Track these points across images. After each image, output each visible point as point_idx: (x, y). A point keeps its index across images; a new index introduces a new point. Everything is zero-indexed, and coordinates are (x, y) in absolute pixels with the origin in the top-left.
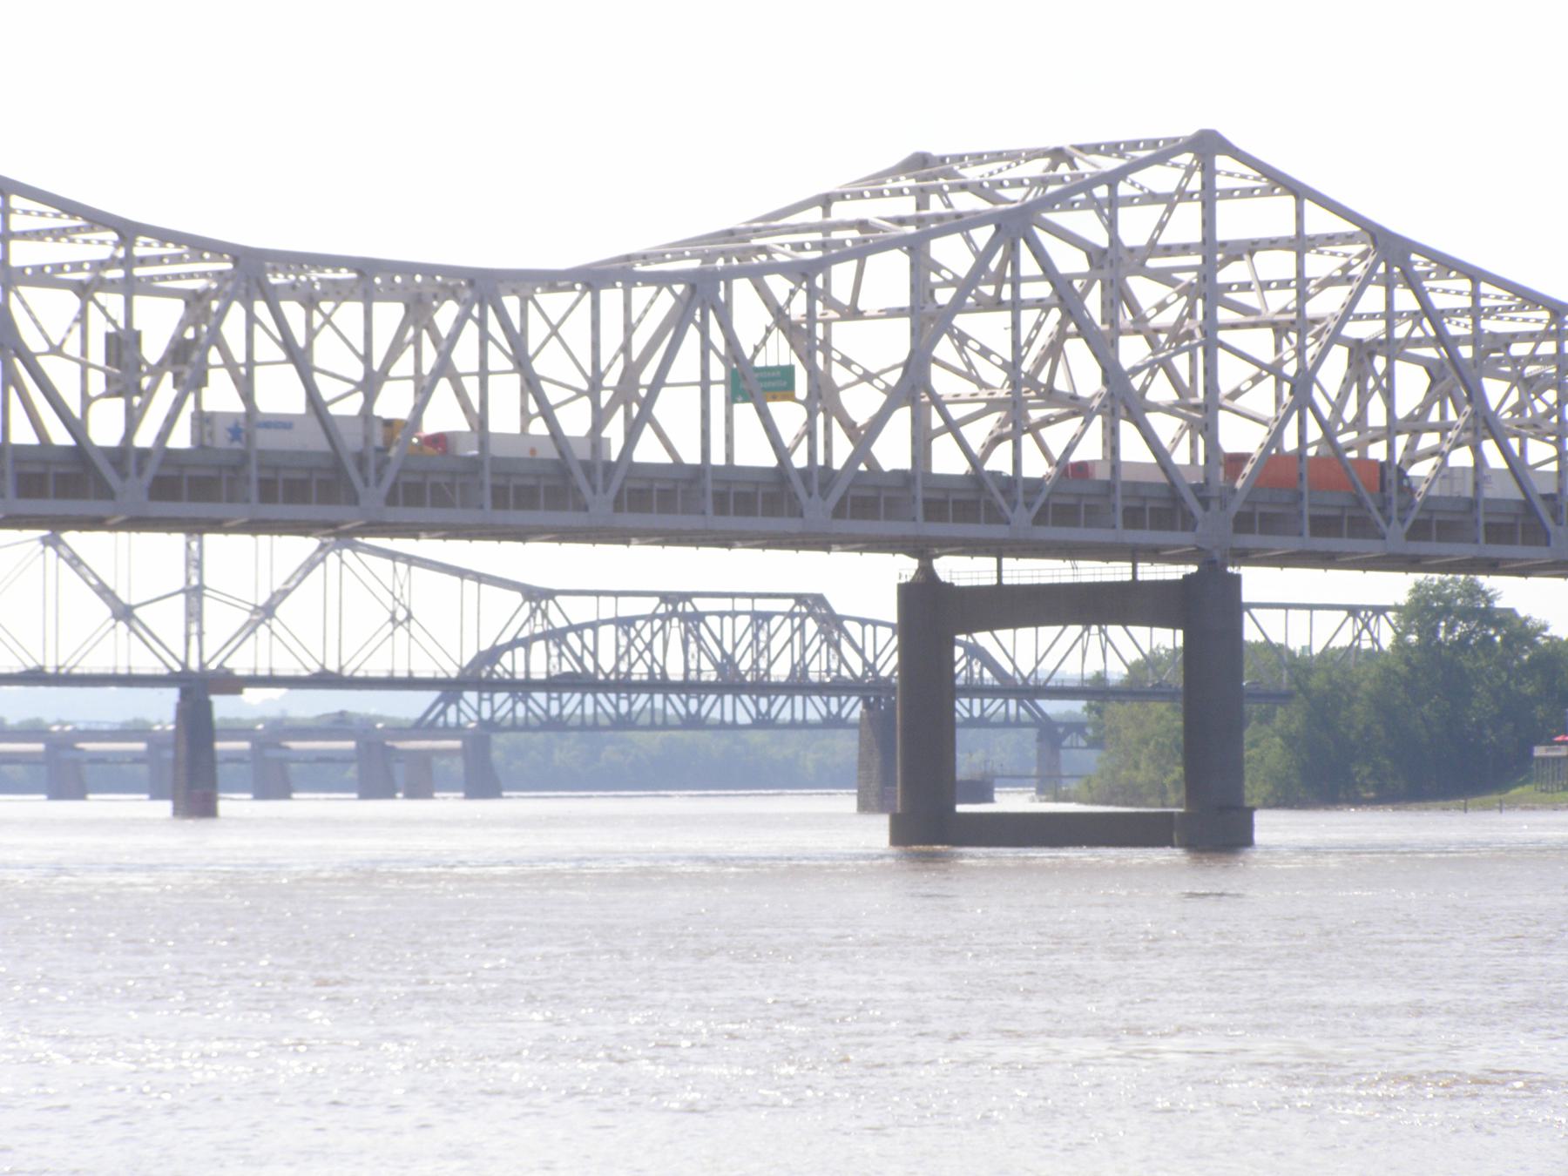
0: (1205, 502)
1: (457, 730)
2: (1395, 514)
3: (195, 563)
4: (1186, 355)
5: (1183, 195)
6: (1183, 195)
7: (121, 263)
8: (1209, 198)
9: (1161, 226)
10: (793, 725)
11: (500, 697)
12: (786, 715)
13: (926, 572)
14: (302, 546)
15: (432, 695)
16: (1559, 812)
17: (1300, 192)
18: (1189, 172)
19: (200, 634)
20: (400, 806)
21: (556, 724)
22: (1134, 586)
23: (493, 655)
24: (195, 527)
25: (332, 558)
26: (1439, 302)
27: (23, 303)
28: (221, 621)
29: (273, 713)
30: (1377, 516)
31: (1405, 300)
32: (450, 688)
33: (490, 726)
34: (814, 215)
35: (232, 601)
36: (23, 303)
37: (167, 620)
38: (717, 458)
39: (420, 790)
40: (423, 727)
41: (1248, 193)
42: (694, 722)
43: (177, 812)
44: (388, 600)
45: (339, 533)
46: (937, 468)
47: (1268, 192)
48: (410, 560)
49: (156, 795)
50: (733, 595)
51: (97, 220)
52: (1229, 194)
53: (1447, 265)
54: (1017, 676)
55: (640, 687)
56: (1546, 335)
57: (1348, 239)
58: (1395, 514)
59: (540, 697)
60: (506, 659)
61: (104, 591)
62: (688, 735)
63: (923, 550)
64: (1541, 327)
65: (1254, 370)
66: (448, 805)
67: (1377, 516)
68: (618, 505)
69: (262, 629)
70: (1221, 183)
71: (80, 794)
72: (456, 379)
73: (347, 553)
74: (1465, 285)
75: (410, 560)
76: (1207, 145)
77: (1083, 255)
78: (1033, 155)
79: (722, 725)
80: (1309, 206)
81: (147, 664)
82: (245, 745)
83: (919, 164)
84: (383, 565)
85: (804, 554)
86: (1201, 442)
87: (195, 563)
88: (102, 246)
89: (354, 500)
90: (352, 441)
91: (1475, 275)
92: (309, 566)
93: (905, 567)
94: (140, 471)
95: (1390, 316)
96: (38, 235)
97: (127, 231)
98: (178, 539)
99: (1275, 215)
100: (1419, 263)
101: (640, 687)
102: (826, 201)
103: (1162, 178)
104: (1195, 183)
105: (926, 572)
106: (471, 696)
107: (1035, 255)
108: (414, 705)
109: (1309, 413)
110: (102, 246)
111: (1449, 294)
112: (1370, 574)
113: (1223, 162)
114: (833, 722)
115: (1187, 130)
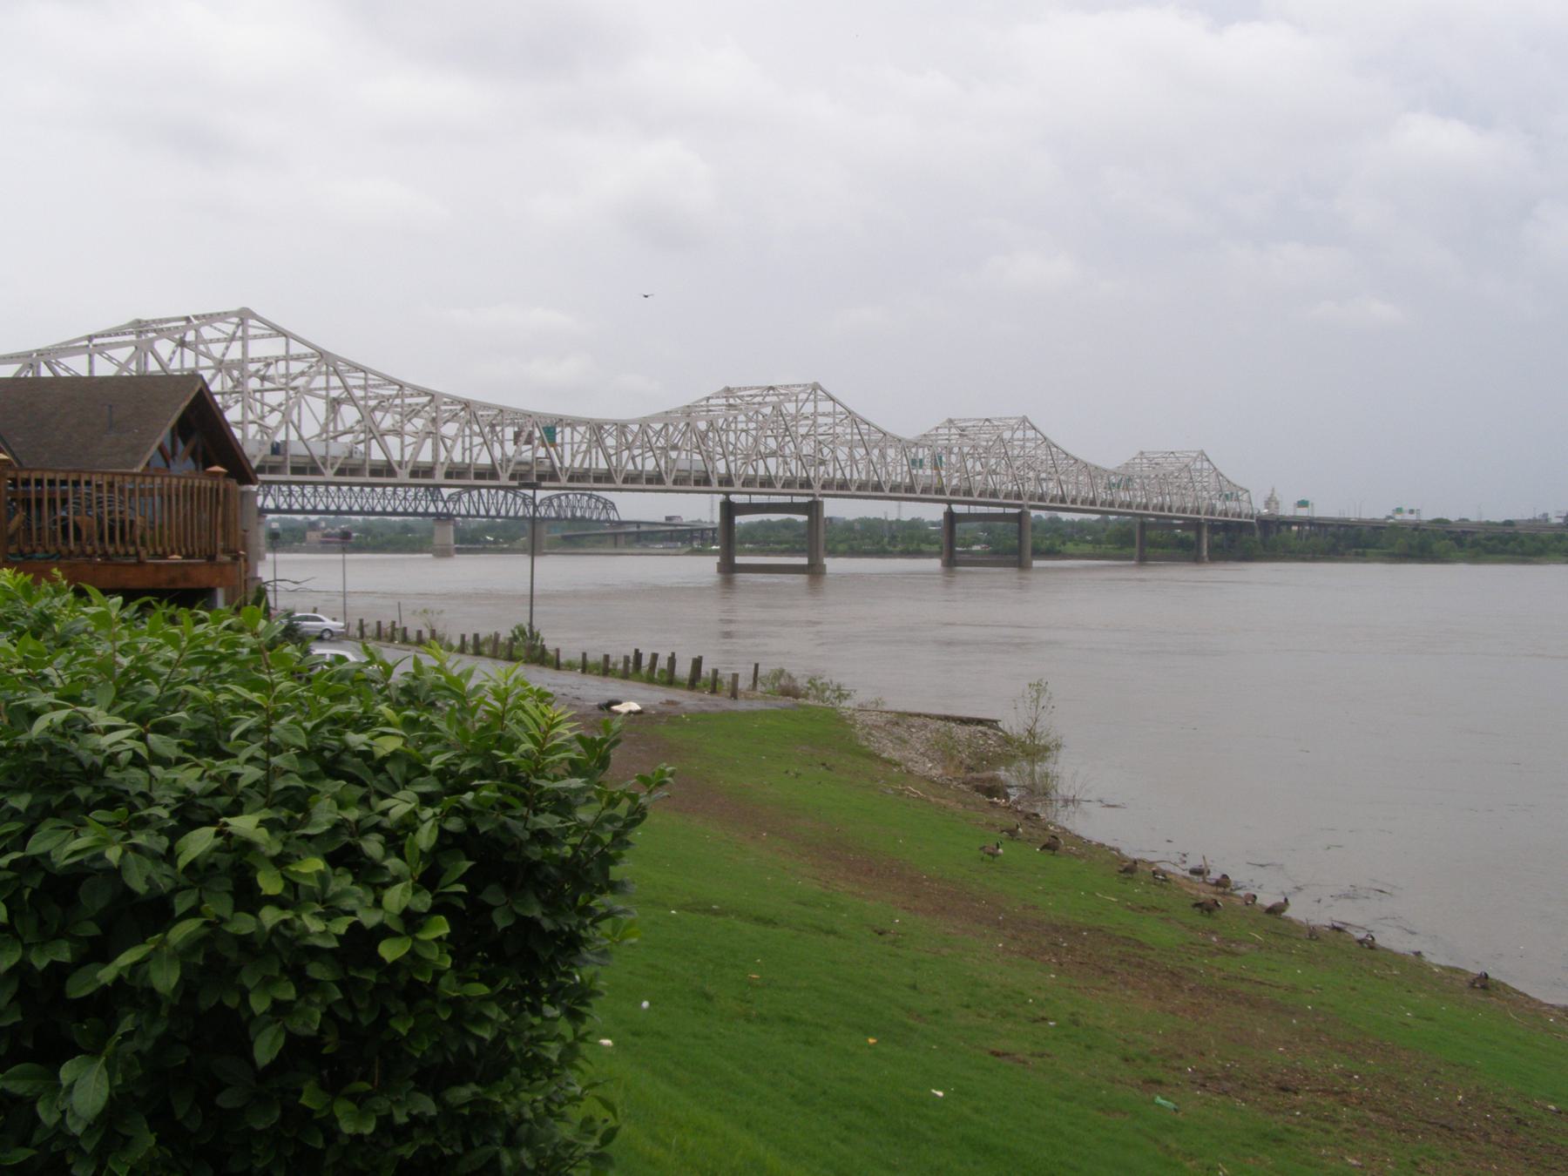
2: (329, 466)
5: (232, 338)
8: (244, 339)
13: (950, 508)
16: (1201, 567)
18: (810, 394)
22: (1004, 514)
27: (308, 406)
31: (335, 381)
36: (308, 406)
38: (594, 466)
41: (263, 336)
47: (277, 336)
53: (357, 368)
56: (397, 396)
57: (313, 356)
58: (329, 466)
64: (395, 392)
67: (322, 467)
70: (252, 332)
74: (362, 375)
76: (244, 316)
78: (758, 388)
95: (852, 434)
99: (275, 347)
100: (342, 367)
107: (157, 359)
111: (354, 380)
113: (252, 322)
115: (235, 308)
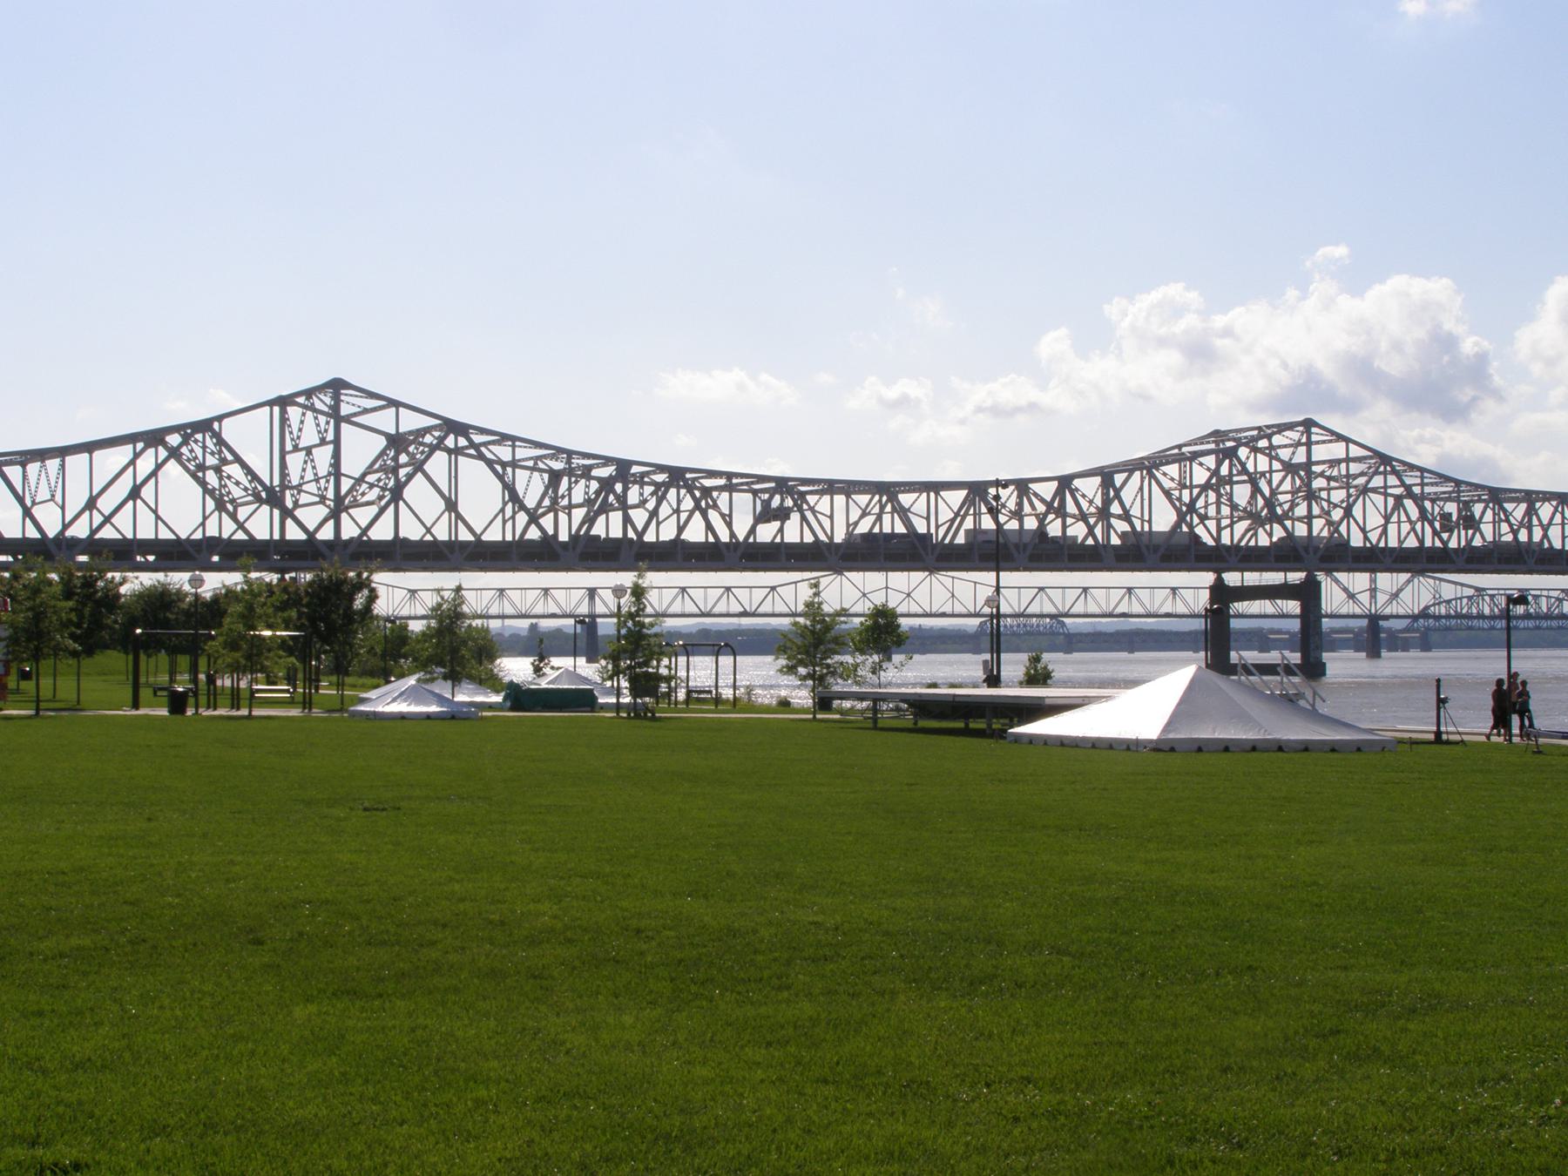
0: (1018, 550)
1: (1417, 630)
3: (1373, 581)
4: (1482, 505)
5: (1299, 444)
6: (1299, 444)
7: (1457, 492)
8: (1309, 444)
9: (1294, 453)
10: (1524, 629)
11: (1431, 621)
12: (1522, 626)
13: (1219, 581)
14: (1404, 577)
15: (1410, 620)
17: (1347, 440)
19: (1376, 603)
20: (1399, 654)
21: (1448, 629)
23: (1427, 608)
24: (1373, 571)
25: (1416, 580)
26: (1408, 481)
28: (1382, 598)
29: (1270, 626)
30: (922, 552)
32: (1415, 618)
33: (1428, 629)
34: (1176, 451)
35: (1384, 592)
37: (1364, 598)
39: (1405, 649)
40: (1406, 630)
42: (1470, 628)
43: (1367, 656)
44: (1432, 591)
45: (1421, 572)
46: (1112, 543)
47: (1337, 441)
48: (1441, 580)
49: (1357, 650)
50: (1498, 589)
51: (1448, 479)
52: (1317, 443)
54: (801, 620)
55: (1475, 618)
57: (1371, 458)
59: (1444, 621)
60: (1432, 608)
61: (1345, 590)
62: (1537, 632)
63: (1218, 571)
65: (305, 480)
66: (1414, 653)
67: (922, 552)
68: (1536, 563)
69: (1394, 602)
70: (1314, 438)
71: (1269, 652)
72: (1541, 524)
73: (1421, 578)
74: (1418, 474)
75: (1441, 580)
77: (383, 438)
79: (1479, 629)
80: (1351, 445)
81: (1358, 611)
82: (1351, 636)
83: (1216, 433)
84: (1431, 581)
85: (694, 574)
86: (453, 514)
87: (1373, 581)
88: (1449, 488)
89: (1525, 563)
90: (1015, 539)
91: (1422, 470)
92: (1408, 581)
93: (1208, 578)
94: (1024, 550)
96: (1432, 484)
97: (1458, 483)
98: (1368, 575)
99: (1338, 450)
101: (1475, 618)
102: (1180, 447)
103: (1293, 435)
104: (1304, 440)
105: (1219, 581)
106: (1422, 620)
108: (1404, 623)
109: (1351, 520)
110: (1449, 488)
112: (619, 573)
113: (1314, 430)
114: (1492, 628)
